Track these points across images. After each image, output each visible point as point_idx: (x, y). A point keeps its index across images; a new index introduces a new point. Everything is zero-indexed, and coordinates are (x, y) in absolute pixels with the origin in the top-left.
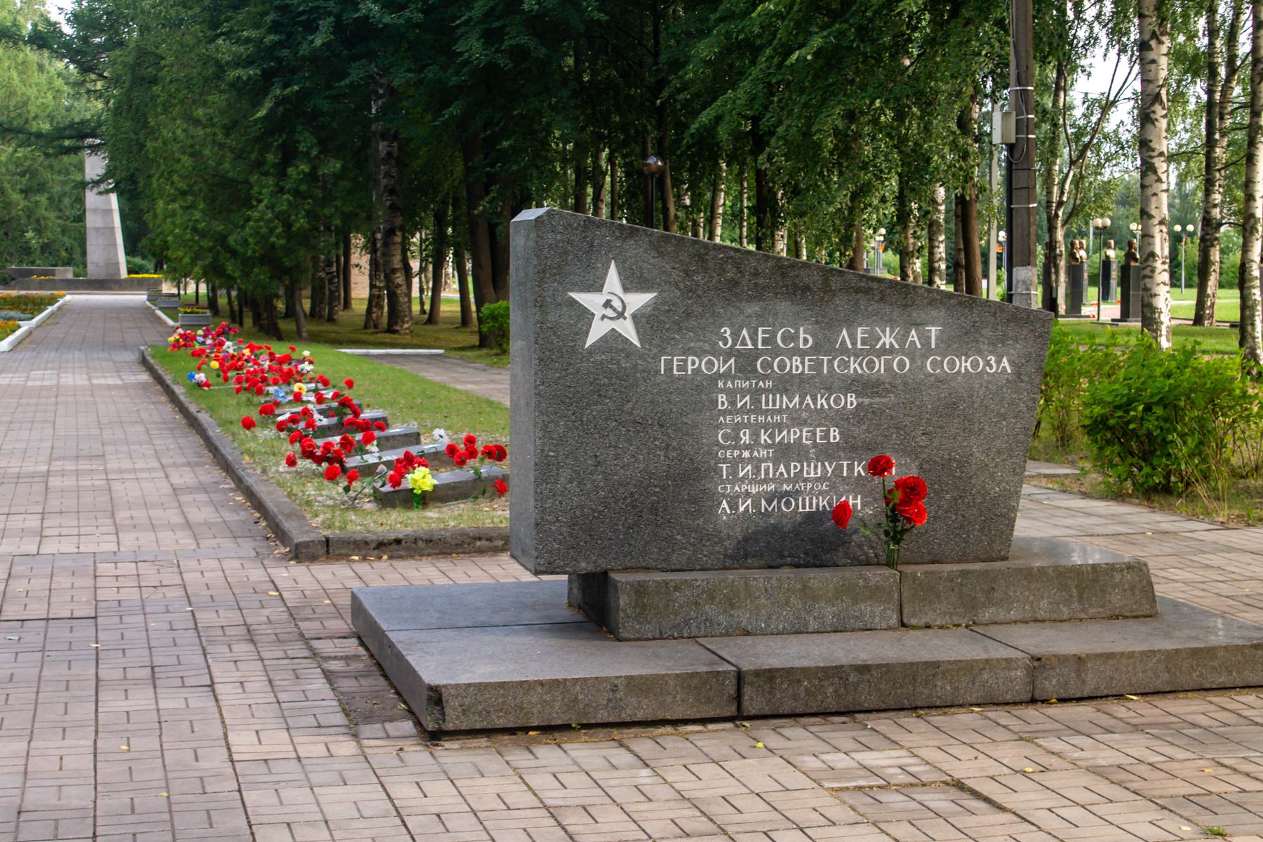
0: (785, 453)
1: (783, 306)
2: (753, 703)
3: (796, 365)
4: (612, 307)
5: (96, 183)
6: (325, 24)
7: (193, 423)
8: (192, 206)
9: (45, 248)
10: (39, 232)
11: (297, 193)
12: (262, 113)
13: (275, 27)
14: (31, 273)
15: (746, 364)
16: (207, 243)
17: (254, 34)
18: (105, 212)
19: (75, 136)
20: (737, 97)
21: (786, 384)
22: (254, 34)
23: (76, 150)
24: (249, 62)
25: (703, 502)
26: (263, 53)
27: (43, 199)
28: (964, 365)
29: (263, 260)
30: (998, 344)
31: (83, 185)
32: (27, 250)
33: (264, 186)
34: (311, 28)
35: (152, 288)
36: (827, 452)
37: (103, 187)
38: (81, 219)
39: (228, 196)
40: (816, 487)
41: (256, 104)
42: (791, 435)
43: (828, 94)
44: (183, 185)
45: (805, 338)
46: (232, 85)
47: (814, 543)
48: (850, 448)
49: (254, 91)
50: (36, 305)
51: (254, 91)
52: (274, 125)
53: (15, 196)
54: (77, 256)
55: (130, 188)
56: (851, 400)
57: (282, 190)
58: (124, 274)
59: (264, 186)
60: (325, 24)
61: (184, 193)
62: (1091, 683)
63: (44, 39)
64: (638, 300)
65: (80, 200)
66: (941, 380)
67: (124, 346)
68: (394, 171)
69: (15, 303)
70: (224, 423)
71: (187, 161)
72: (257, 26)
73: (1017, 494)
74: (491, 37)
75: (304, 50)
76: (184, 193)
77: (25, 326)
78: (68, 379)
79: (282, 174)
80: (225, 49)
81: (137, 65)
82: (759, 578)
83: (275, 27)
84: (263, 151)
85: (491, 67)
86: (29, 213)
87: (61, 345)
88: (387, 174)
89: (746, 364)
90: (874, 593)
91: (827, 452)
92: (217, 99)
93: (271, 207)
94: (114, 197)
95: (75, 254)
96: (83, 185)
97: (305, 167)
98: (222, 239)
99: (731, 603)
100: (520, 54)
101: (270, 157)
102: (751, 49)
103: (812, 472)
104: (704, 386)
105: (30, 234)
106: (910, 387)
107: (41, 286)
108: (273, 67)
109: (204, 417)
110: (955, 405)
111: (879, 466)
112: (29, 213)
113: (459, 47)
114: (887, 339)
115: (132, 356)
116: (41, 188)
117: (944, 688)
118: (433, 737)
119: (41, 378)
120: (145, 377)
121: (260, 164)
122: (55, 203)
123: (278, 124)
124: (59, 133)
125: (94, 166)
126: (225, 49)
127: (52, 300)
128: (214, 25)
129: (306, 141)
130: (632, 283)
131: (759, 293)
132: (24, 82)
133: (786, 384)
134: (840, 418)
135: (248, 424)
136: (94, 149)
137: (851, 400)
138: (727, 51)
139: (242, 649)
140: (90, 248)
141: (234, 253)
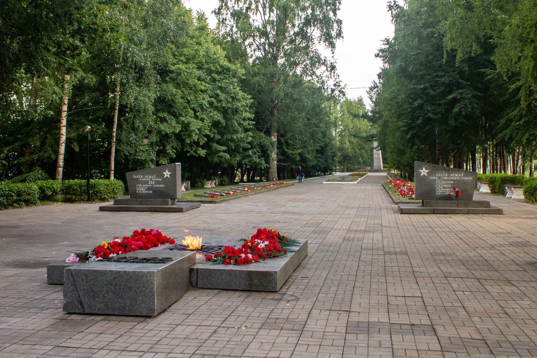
0: (444, 188)
1: (444, 172)
2: (435, 212)
3: (445, 178)
4: (424, 172)
5: (376, 148)
6: (421, 118)
7: (388, 193)
8: (393, 155)
9: (364, 162)
10: (362, 158)
11: (414, 152)
12: (408, 137)
13: (410, 119)
14: (360, 168)
15: (439, 178)
16: (396, 162)
17: (406, 121)
18: (378, 155)
19: (370, 138)
20: (508, 131)
21: (444, 180)
22: (406, 121)
23: (371, 140)
24: (405, 126)
25: (435, 193)
26: (408, 124)
27: (364, 151)
28: (466, 178)
29: (408, 166)
30: (470, 176)
31: (373, 148)
32: (359, 163)
33: (408, 151)
34: (418, 119)
35: (389, 171)
36: (449, 188)
37: (377, 149)
38: (372, 155)
39: (401, 153)
40: (448, 191)
41: (407, 134)
42: (445, 186)
43: (526, 131)
44: (392, 151)
45: (446, 175)
46: (402, 131)
47: (448, 198)
48: (452, 187)
49: (407, 132)
50: (361, 175)
51: (407, 132)
52: (410, 139)
53: (358, 151)
54: (371, 164)
55: (383, 149)
56: (452, 182)
57: (411, 151)
58: (382, 168)
59: (408, 151)
60: (421, 118)
61: (392, 152)
62: (476, 212)
63: (365, 116)
64: (427, 171)
65: (372, 151)
66: (463, 180)
67: (380, 183)
68: (440, 146)
69: (357, 175)
70: (392, 192)
71: (392, 146)
72: (407, 119)
73: (473, 193)
74: (456, 120)
75: (416, 123)
76: (392, 152)
77: (360, 179)
78: (368, 188)
79: (412, 148)
80: (400, 124)
81: (385, 123)
82: (440, 201)
83: (410, 119)
84: (408, 144)
85: (456, 126)
86: (361, 154)
87: (367, 183)
88: (438, 147)
89: (439, 178)
90: (454, 203)
91: (449, 188)
92: (399, 133)
93: (409, 155)
94: (380, 151)
95: (371, 164)
96: (373, 148)
97: (416, 147)
98: (399, 161)
99: (437, 204)
100: (462, 123)
101: (409, 145)
102: (512, 120)
103: (448, 190)
104: (435, 180)
105: (360, 159)
106: (459, 181)
107: (363, 171)
108: (410, 128)
109: (390, 192)
110: (465, 183)
111: (454, 189)
112: (361, 154)
113: (449, 122)
114: (456, 175)
115: (381, 185)
116: (363, 148)
117: (458, 212)
118: (402, 213)
119: (362, 187)
120: (382, 187)
121: (407, 146)
122: (366, 152)
123: (413, 136)
124: (368, 137)
125: (375, 144)
126: (400, 124)
127: (365, 174)
128: (399, 118)
129: (417, 141)
130: (426, 169)
131: (441, 170)
132: (360, 124)
133: (444, 180)
134: (451, 184)
135: (395, 192)
136: (375, 140)
137: (452, 182)
138: (506, 121)
139: (386, 210)
140: (374, 163)
141: (402, 164)
